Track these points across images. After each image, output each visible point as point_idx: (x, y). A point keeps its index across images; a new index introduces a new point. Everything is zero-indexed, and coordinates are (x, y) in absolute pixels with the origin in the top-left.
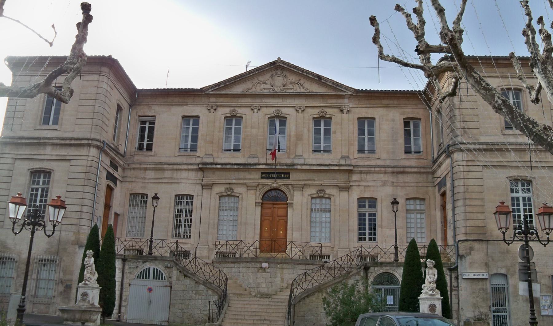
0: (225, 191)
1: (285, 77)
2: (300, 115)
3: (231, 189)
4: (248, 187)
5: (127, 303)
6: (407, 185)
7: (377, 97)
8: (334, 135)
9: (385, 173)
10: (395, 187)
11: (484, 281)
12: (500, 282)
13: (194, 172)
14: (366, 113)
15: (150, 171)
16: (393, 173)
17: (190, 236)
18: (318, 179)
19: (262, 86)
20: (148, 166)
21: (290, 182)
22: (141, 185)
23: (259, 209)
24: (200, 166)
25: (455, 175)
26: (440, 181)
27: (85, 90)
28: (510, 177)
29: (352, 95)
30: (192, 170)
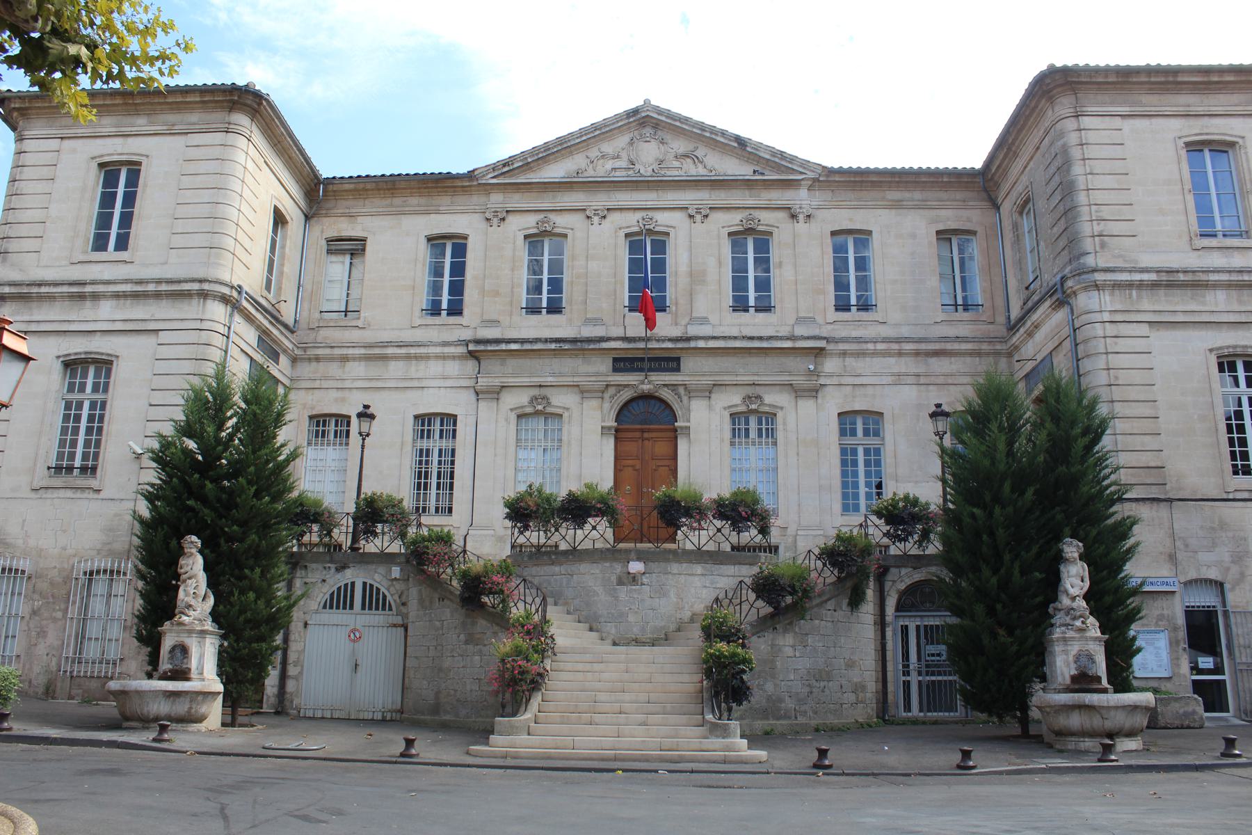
0: (531, 402)
1: (662, 142)
2: (699, 227)
3: (543, 398)
4: (583, 392)
5: (299, 669)
6: (950, 381)
7: (875, 185)
8: (777, 272)
9: (900, 354)
10: (923, 387)
11: (1169, 597)
12: (1204, 599)
13: (457, 362)
14: (851, 220)
15: (357, 363)
16: (917, 354)
17: (450, 510)
18: (746, 371)
19: (609, 165)
20: (351, 351)
21: (680, 378)
22: (334, 394)
23: (611, 442)
24: (471, 347)
25: (1080, 348)
26: (1034, 369)
27: (191, 168)
28: (1218, 349)
29: (818, 180)
30: (454, 358)
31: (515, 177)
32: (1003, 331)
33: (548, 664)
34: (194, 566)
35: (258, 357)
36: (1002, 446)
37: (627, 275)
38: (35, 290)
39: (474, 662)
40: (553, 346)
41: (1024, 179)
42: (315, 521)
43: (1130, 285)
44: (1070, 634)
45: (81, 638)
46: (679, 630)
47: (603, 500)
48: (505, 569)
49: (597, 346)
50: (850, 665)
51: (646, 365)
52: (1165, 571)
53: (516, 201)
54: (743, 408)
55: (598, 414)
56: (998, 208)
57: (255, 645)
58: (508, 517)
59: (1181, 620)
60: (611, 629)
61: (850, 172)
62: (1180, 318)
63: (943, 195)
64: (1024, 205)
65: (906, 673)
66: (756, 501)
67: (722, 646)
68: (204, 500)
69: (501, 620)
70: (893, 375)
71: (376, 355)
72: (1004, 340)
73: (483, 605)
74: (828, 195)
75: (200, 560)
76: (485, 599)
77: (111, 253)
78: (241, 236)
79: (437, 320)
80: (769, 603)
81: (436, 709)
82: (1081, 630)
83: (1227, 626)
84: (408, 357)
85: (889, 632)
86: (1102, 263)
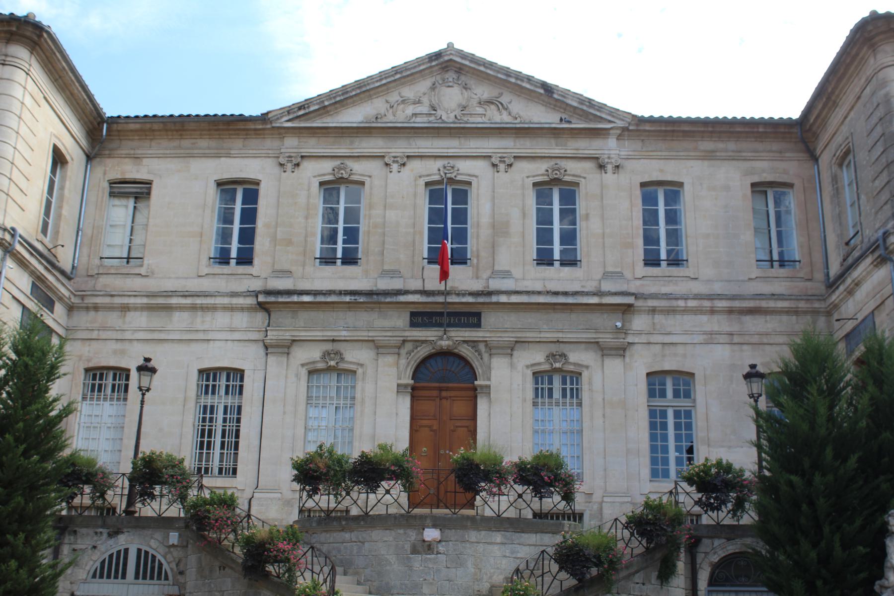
1: (466, 87)
2: (503, 177)
4: (379, 347)
9: (712, 311)
15: (138, 313)
16: (730, 311)
17: (235, 471)
19: (410, 110)
20: (132, 300)
23: (405, 403)
24: (261, 298)
30: (242, 309)
31: (311, 120)
32: (821, 288)
35: (32, 305)
40: (347, 299)
41: (845, 129)
42: (88, 482)
47: (397, 462)
48: (292, 535)
49: (394, 299)
51: (445, 320)
53: (312, 146)
54: (546, 367)
55: (393, 371)
56: (815, 159)
58: (297, 479)
61: (661, 121)
63: (758, 146)
64: (844, 157)
66: (560, 466)
70: (705, 333)
71: (160, 305)
72: (822, 298)
73: (268, 574)
74: (638, 145)
79: (225, 269)
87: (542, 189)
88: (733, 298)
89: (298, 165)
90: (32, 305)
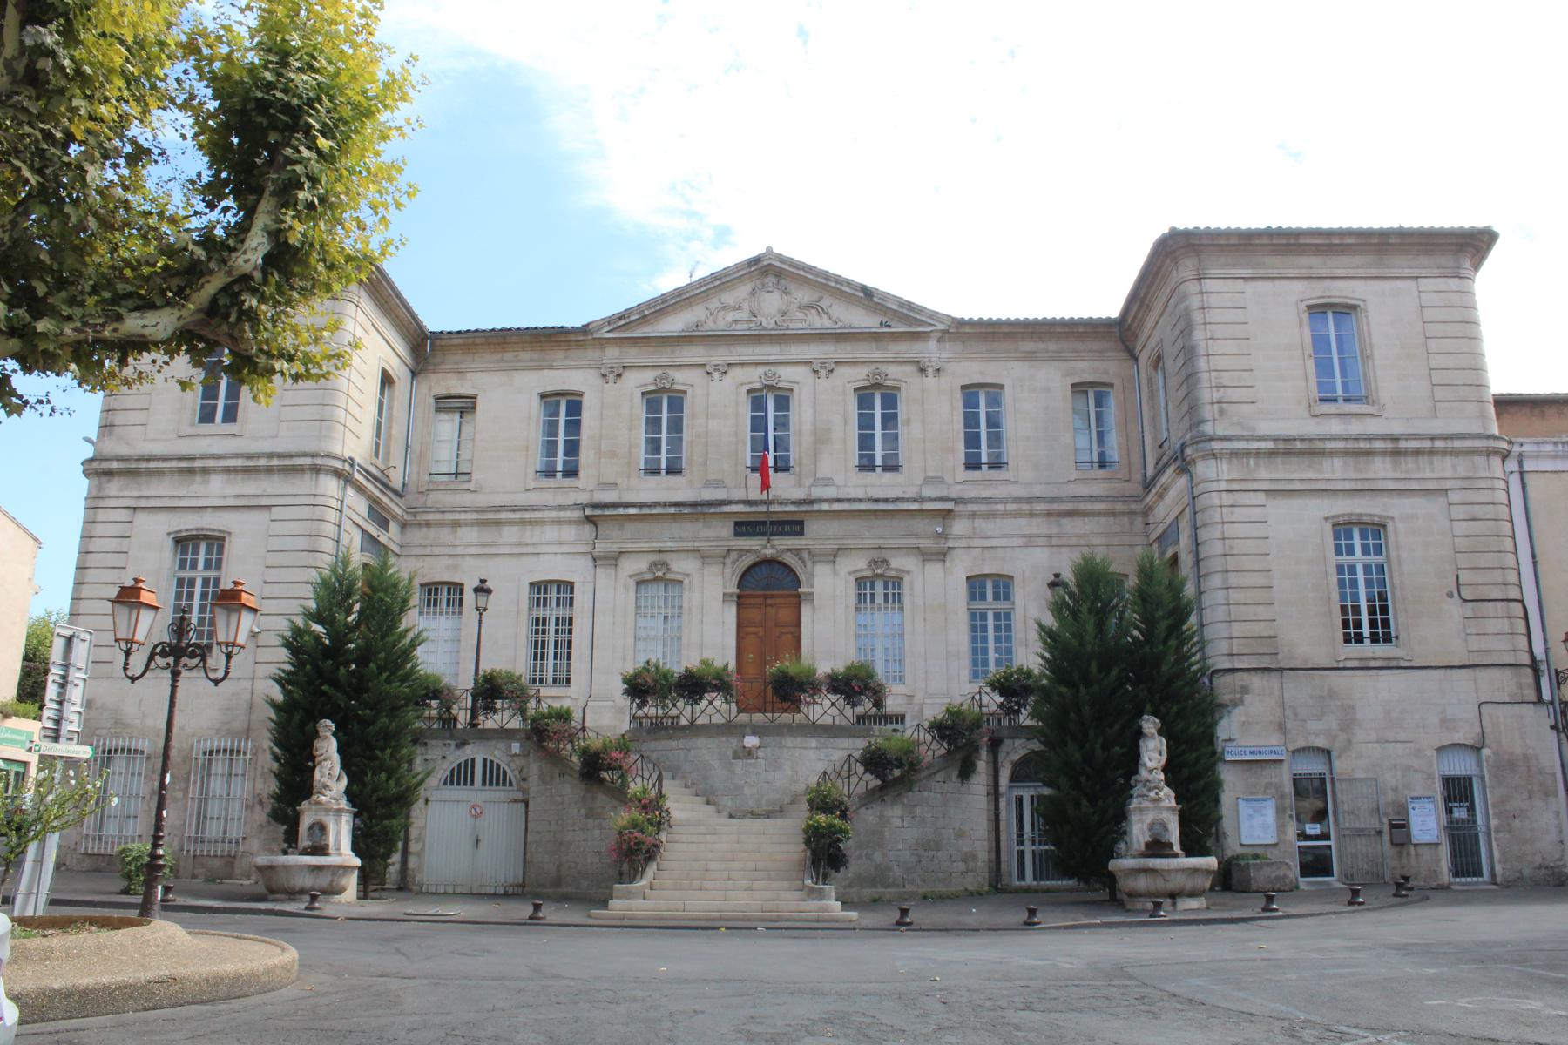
0: (650, 568)
1: (786, 292)
2: (824, 383)
4: (704, 557)
9: (1032, 515)
12: (1313, 767)
15: (468, 529)
16: (1049, 514)
17: (568, 681)
19: (730, 317)
20: (463, 516)
22: (445, 561)
23: (732, 611)
24: (588, 512)
25: (1199, 516)
30: (570, 522)
31: (631, 330)
32: (1139, 489)
33: (663, 836)
34: (328, 748)
35: (373, 530)
36: (1090, 628)
37: (749, 434)
38: (143, 465)
39: (595, 832)
40: (672, 510)
41: (1157, 333)
42: (435, 698)
43: (1247, 453)
44: (1146, 804)
45: (202, 817)
46: (793, 802)
47: (718, 677)
48: (624, 745)
49: (718, 510)
50: (960, 835)
51: (768, 529)
52: (1274, 740)
53: (633, 356)
54: (868, 573)
55: (719, 581)
56: (1136, 359)
57: (386, 822)
58: (627, 692)
59: (1288, 788)
60: (727, 802)
61: (981, 323)
62: (1297, 486)
63: (1079, 346)
64: (1158, 361)
65: (1021, 843)
66: (871, 675)
67: (822, 819)
68: (335, 684)
69: (619, 793)
70: (1024, 536)
71: (489, 519)
72: (1138, 499)
73: (602, 781)
74: (958, 347)
75: (334, 743)
76: (604, 775)
77: (218, 425)
78: (352, 406)
79: (551, 482)
80: (878, 776)
81: (557, 882)
82: (1156, 801)
83: (1334, 793)
84: (523, 522)
85: (1003, 803)
86: (1220, 431)
87: (864, 397)
88: (1053, 500)
89: (620, 375)
90: (373, 530)
